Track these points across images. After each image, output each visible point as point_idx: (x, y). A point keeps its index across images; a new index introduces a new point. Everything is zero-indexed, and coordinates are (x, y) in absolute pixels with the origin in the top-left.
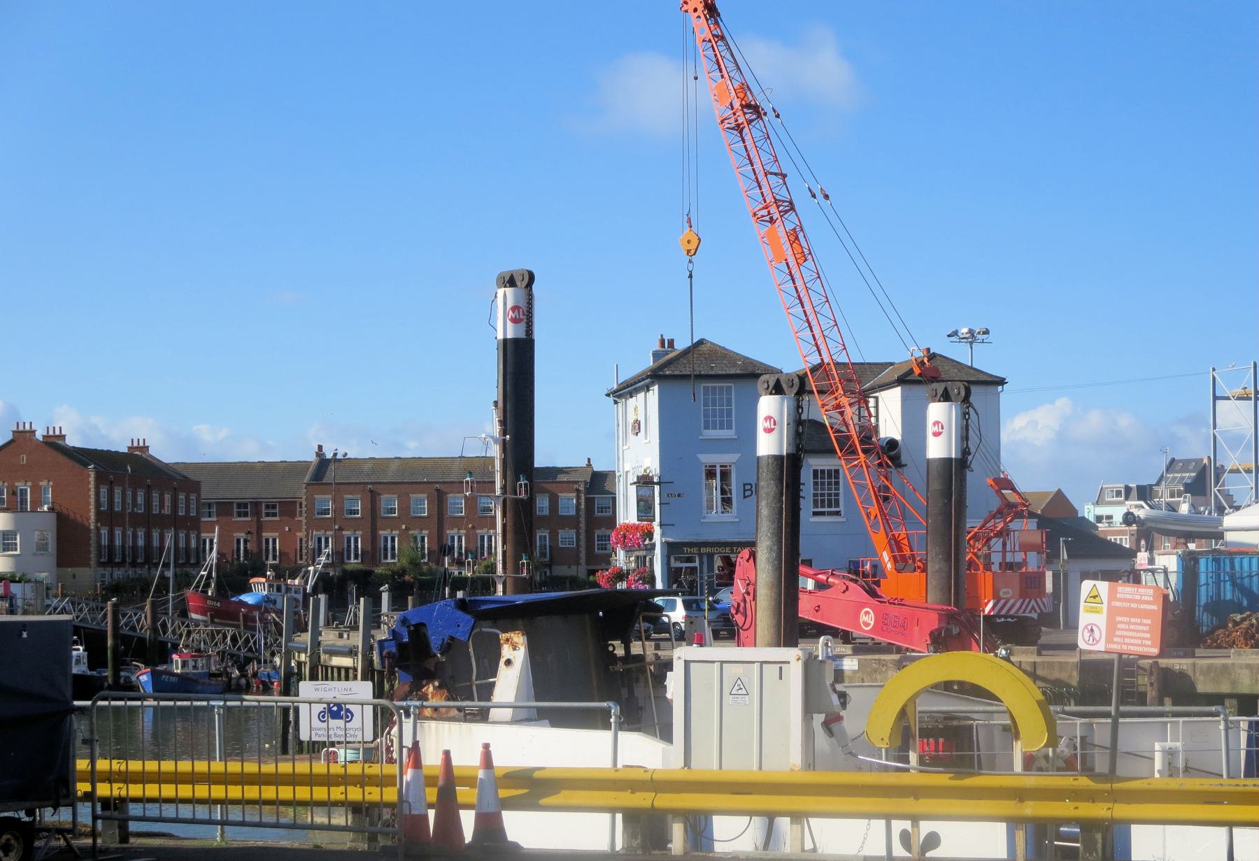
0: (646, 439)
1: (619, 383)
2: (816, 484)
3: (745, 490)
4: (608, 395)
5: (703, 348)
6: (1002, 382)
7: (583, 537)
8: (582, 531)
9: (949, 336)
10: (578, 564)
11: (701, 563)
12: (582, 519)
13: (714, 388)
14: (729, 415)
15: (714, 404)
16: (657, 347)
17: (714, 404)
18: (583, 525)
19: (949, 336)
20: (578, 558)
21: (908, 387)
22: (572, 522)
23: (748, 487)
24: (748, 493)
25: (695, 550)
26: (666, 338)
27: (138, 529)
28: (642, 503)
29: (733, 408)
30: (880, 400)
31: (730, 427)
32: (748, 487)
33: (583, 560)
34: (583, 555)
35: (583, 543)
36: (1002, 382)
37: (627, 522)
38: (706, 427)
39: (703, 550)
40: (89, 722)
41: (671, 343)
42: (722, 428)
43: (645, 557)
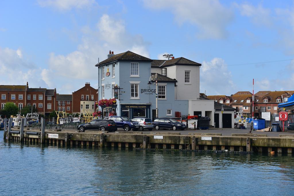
0: (112, 77)
1: (99, 62)
2: (159, 90)
3: (141, 91)
4: (96, 66)
5: (127, 54)
6: (200, 65)
7: (44, 105)
8: (44, 104)
9: (164, 56)
10: (43, 112)
11: (130, 110)
12: (44, 101)
13: (134, 64)
14: (137, 71)
15: (134, 68)
16: (109, 53)
17: (134, 68)
18: (44, 102)
19: (164, 56)
20: (43, 110)
21: (177, 66)
22: (42, 101)
23: (142, 90)
24: (142, 92)
25: (129, 107)
26: (111, 51)
27: (34, 95)
28: (115, 94)
29: (139, 69)
30: (167, 69)
31: (137, 74)
32: (142, 90)
33: (44, 111)
34: (44, 109)
35: (44, 107)
36: (200, 65)
37: (104, 98)
38: (132, 74)
39: (131, 107)
40: (207, 161)
41: (113, 52)
42: (135, 74)
43: (111, 109)
